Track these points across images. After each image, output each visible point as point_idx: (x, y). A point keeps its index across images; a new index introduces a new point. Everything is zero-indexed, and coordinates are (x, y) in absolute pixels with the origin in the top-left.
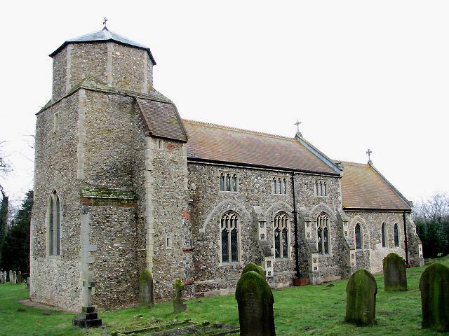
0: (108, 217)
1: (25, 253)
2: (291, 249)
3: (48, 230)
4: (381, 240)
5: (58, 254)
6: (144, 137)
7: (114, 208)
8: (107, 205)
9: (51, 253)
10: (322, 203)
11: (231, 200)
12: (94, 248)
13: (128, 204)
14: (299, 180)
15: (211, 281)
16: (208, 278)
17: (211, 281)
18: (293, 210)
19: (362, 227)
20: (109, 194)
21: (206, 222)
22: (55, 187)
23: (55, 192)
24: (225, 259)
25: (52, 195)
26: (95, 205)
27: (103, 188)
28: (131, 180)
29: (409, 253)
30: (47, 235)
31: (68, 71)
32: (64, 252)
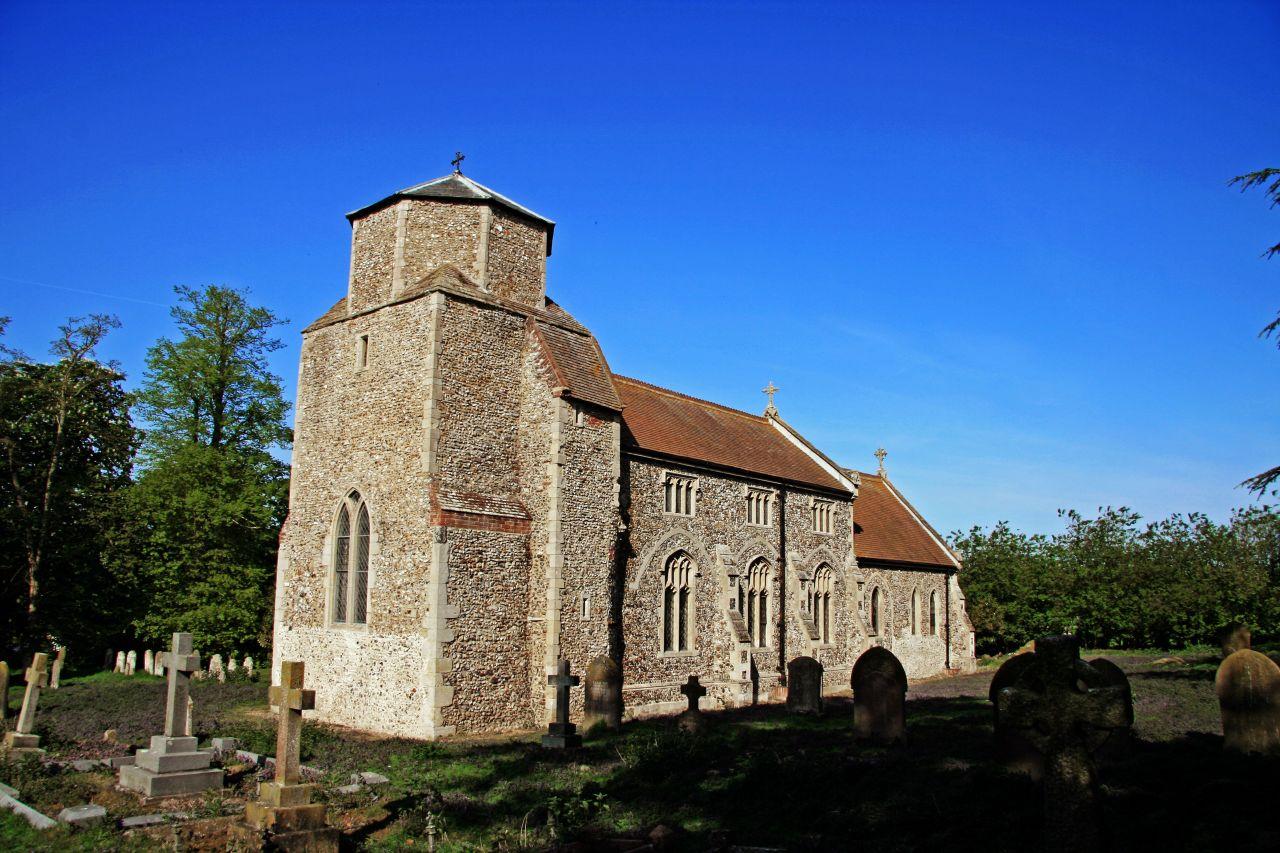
0: (480, 552)
1: (974, 587)
2: (771, 629)
3: (331, 570)
4: (910, 620)
5: (361, 617)
6: (549, 398)
7: (492, 534)
8: (480, 526)
9: (340, 616)
10: (823, 546)
11: (683, 531)
12: (453, 611)
13: (514, 528)
14: (791, 499)
15: (644, 686)
16: (640, 679)
17: (644, 686)
18: (778, 555)
19: (880, 591)
20: (482, 505)
21: (640, 573)
22: (355, 485)
23: (355, 495)
24: (668, 645)
25: (348, 500)
26: (460, 525)
27: (470, 495)
28: (517, 481)
29: (951, 648)
30: (328, 582)
31: (398, 253)
32: (379, 617)
